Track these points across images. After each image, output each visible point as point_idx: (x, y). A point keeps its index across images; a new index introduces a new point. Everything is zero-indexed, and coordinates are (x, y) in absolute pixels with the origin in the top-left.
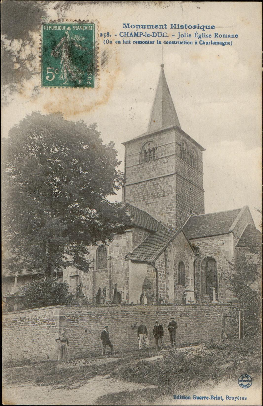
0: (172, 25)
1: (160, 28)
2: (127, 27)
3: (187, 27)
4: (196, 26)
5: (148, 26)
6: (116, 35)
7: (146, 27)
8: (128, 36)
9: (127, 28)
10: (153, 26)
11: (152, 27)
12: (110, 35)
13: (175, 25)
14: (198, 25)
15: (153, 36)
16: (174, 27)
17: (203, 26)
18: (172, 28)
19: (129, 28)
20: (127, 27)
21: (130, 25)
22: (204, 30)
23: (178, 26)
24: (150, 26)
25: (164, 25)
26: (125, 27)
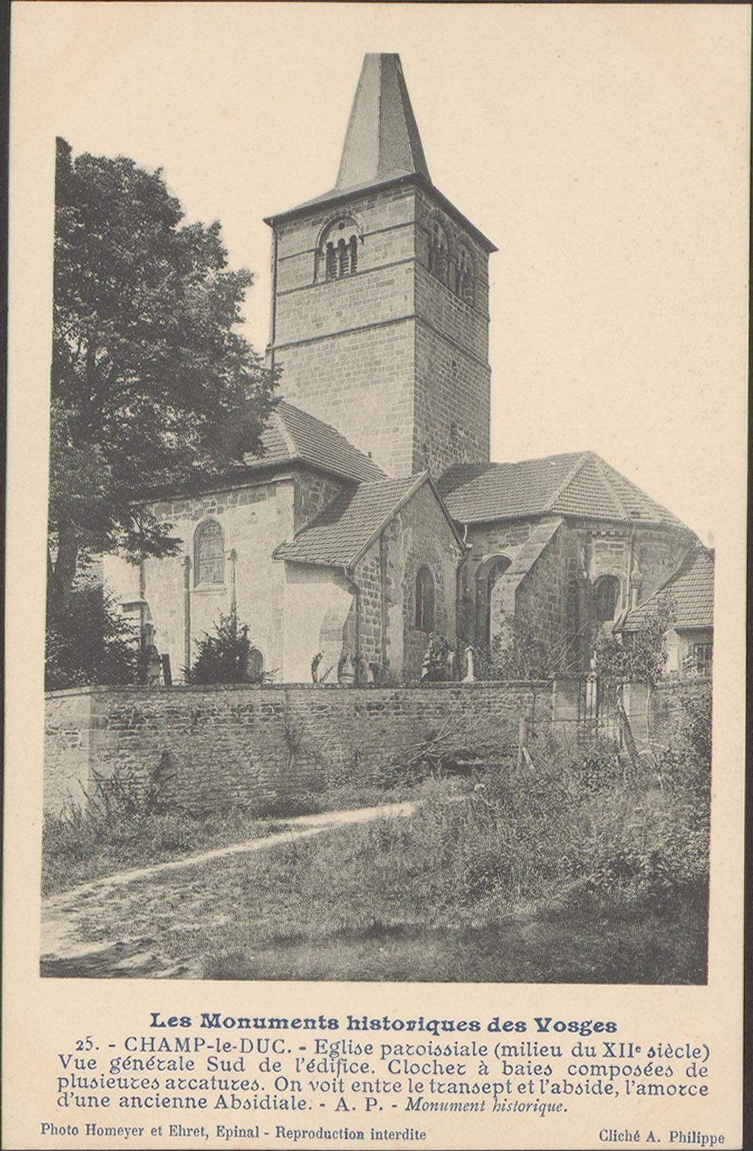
2: (214, 1023)
3: (389, 1025)
4: (414, 1022)
7: (267, 1024)
11: (282, 1024)
14: (365, 1018)
17: (436, 1023)
19: (218, 1025)
20: (214, 1023)
22: (436, 1034)
24: (279, 1021)
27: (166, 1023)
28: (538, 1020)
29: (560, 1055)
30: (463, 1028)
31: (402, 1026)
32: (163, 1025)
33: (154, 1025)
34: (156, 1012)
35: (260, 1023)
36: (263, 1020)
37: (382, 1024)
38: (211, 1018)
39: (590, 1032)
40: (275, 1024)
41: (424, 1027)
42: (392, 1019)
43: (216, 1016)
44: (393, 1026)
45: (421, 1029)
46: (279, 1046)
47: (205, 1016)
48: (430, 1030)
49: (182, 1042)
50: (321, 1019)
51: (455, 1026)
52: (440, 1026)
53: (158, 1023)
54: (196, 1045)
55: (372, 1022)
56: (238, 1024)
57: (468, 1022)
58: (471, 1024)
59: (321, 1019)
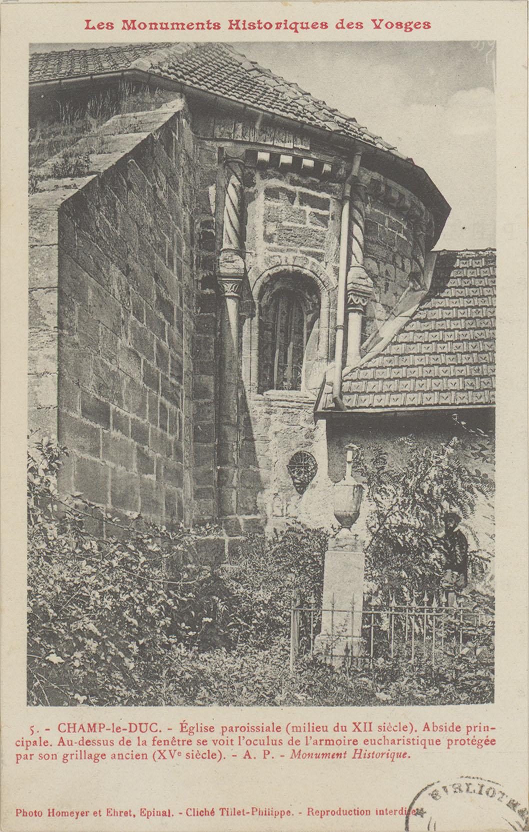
0: (231, 21)
1: (198, 28)
2: (132, 26)
3: (261, 26)
4: (281, 23)
5: (173, 24)
6: (181, 813)
7: (170, 26)
8: (74, 731)
9: (131, 30)
10: (183, 24)
11: (180, 26)
12: (292, 813)
13: (238, 21)
14: (286, 21)
15: (130, 731)
16: (234, 27)
17: (296, 24)
18: (231, 28)
19: (134, 28)
20: (132, 26)
21: (136, 24)
22: (296, 31)
23: (244, 24)
24: (178, 24)
25: (205, 22)
26: (126, 27)
27: (96, 27)
28: (374, 21)
29: (327, 731)
30: (191, 27)
31: (145, 26)
32: (94, 28)
33: (87, 28)
34: (89, 19)
35: (164, 26)
36: (166, 24)
37: (257, 26)
38: (129, 22)
39: (411, 29)
40: (175, 26)
41: (288, 26)
42: (264, 21)
43: (133, 21)
44: (265, 26)
45: (286, 28)
46: (154, 728)
47: (125, 21)
48: (292, 29)
49: (296, 753)
50: (208, 23)
51: (309, 26)
52: (299, 26)
53: (90, 26)
54: (100, 728)
55: (249, 24)
56: (149, 26)
57: (355, 23)
58: (214, 24)
59: (208, 23)
